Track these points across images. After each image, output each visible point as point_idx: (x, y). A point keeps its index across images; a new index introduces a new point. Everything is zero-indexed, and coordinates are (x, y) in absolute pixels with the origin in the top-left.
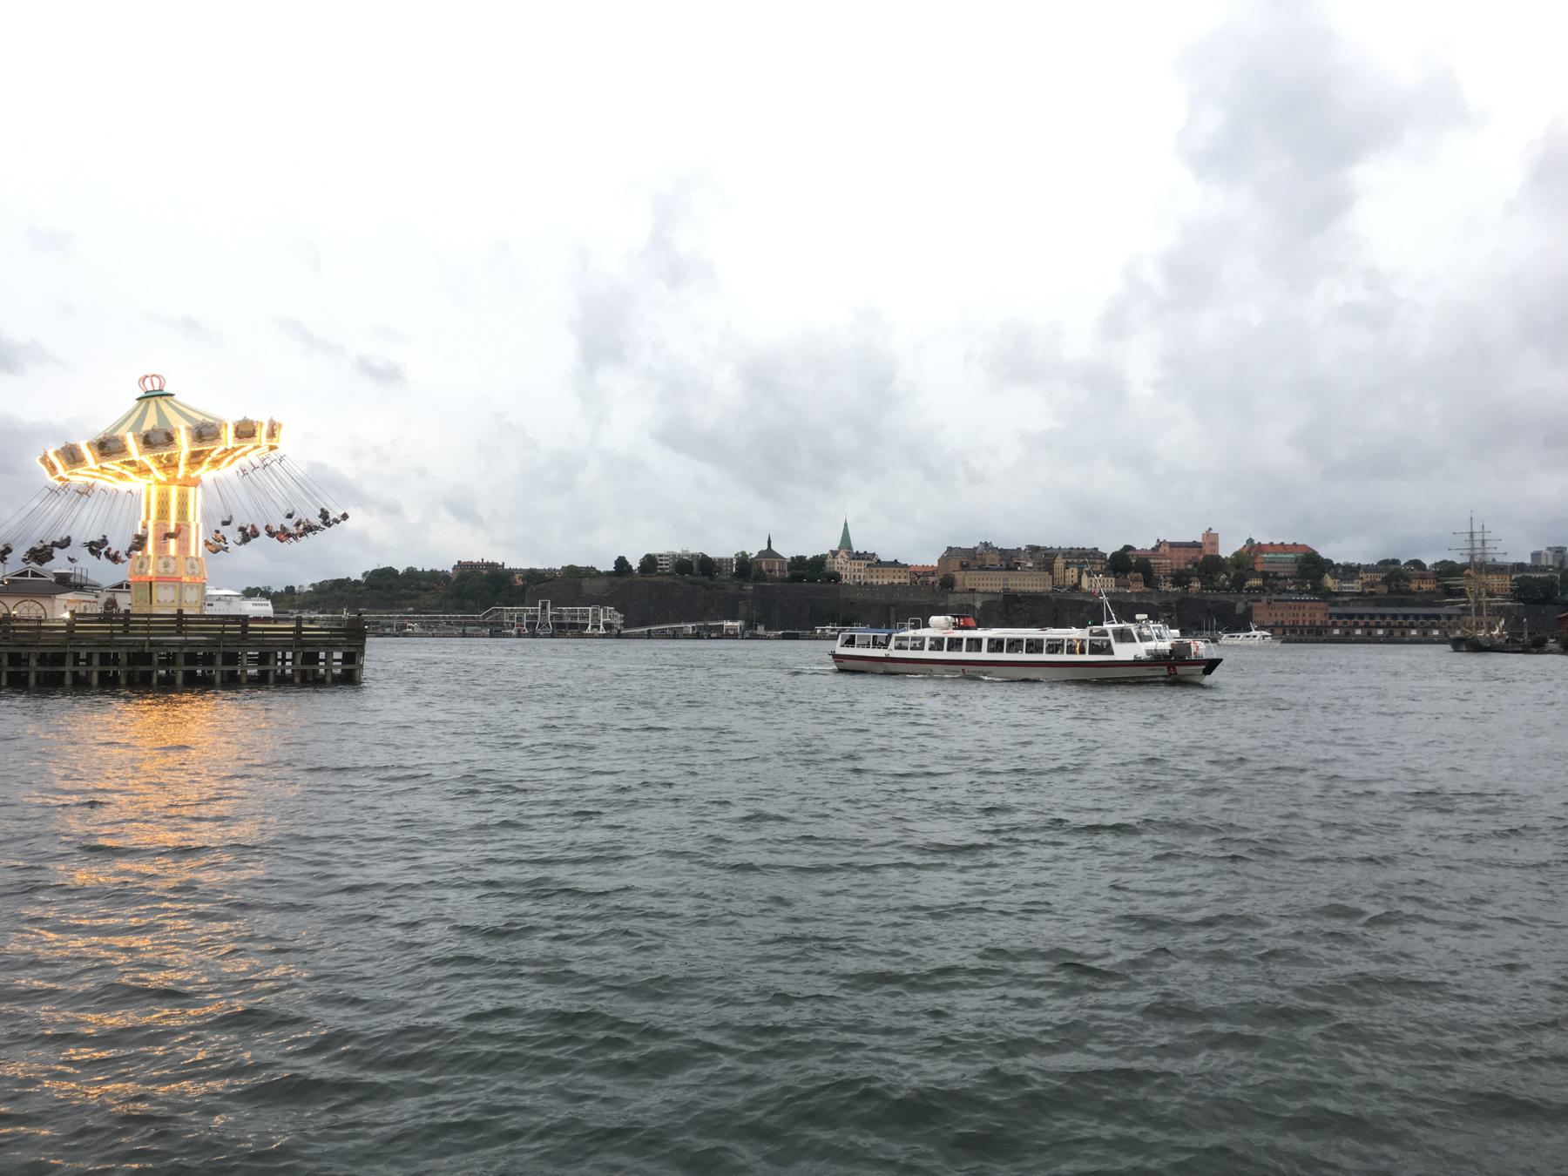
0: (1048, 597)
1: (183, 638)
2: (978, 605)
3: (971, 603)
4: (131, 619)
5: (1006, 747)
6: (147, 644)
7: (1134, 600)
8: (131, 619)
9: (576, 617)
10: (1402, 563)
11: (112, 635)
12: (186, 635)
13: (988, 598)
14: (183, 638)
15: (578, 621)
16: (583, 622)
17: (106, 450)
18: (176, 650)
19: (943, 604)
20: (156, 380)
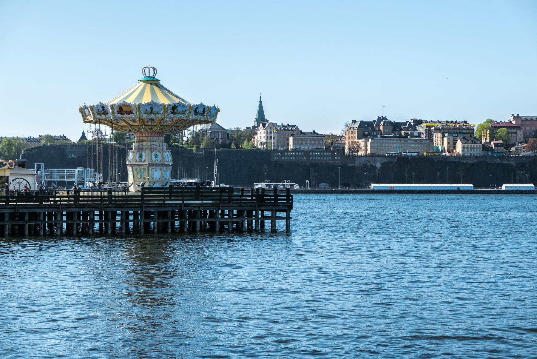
0: (432, 158)
1: (200, 202)
2: (378, 165)
3: (373, 164)
4: (285, 198)
5: (417, 310)
6: (183, 206)
7: (498, 161)
8: (285, 198)
9: (63, 177)
10: (461, 153)
11: (164, 200)
12: (202, 200)
13: (385, 160)
14: (200, 202)
15: (66, 180)
16: (70, 180)
17: (175, 111)
18: (196, 209)
19: (351, 165)
20: (152, 70)
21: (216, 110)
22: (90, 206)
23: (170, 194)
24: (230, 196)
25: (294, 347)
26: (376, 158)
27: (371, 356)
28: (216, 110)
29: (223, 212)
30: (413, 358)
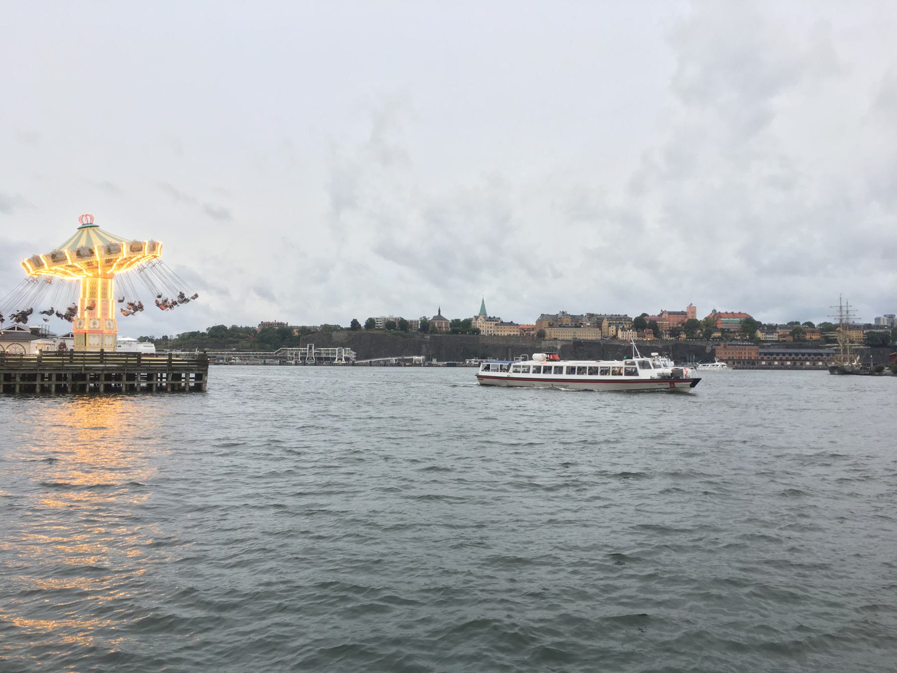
0: (598, 343)
1: (104, 365)
2: (559, 347)
9: (329, 354)
13: (564, 343)
14: (104, 365)
15: (330, 356)
19: (539, 347)
21: (894, 315)
22: (156, 369)
23: (101, 358)
24: (139, 360)
25: (402, 580)
26: (558, 341)
27: (770, 662)
28: (894, 315)
29: (161, 375)
30: (722, 671)
